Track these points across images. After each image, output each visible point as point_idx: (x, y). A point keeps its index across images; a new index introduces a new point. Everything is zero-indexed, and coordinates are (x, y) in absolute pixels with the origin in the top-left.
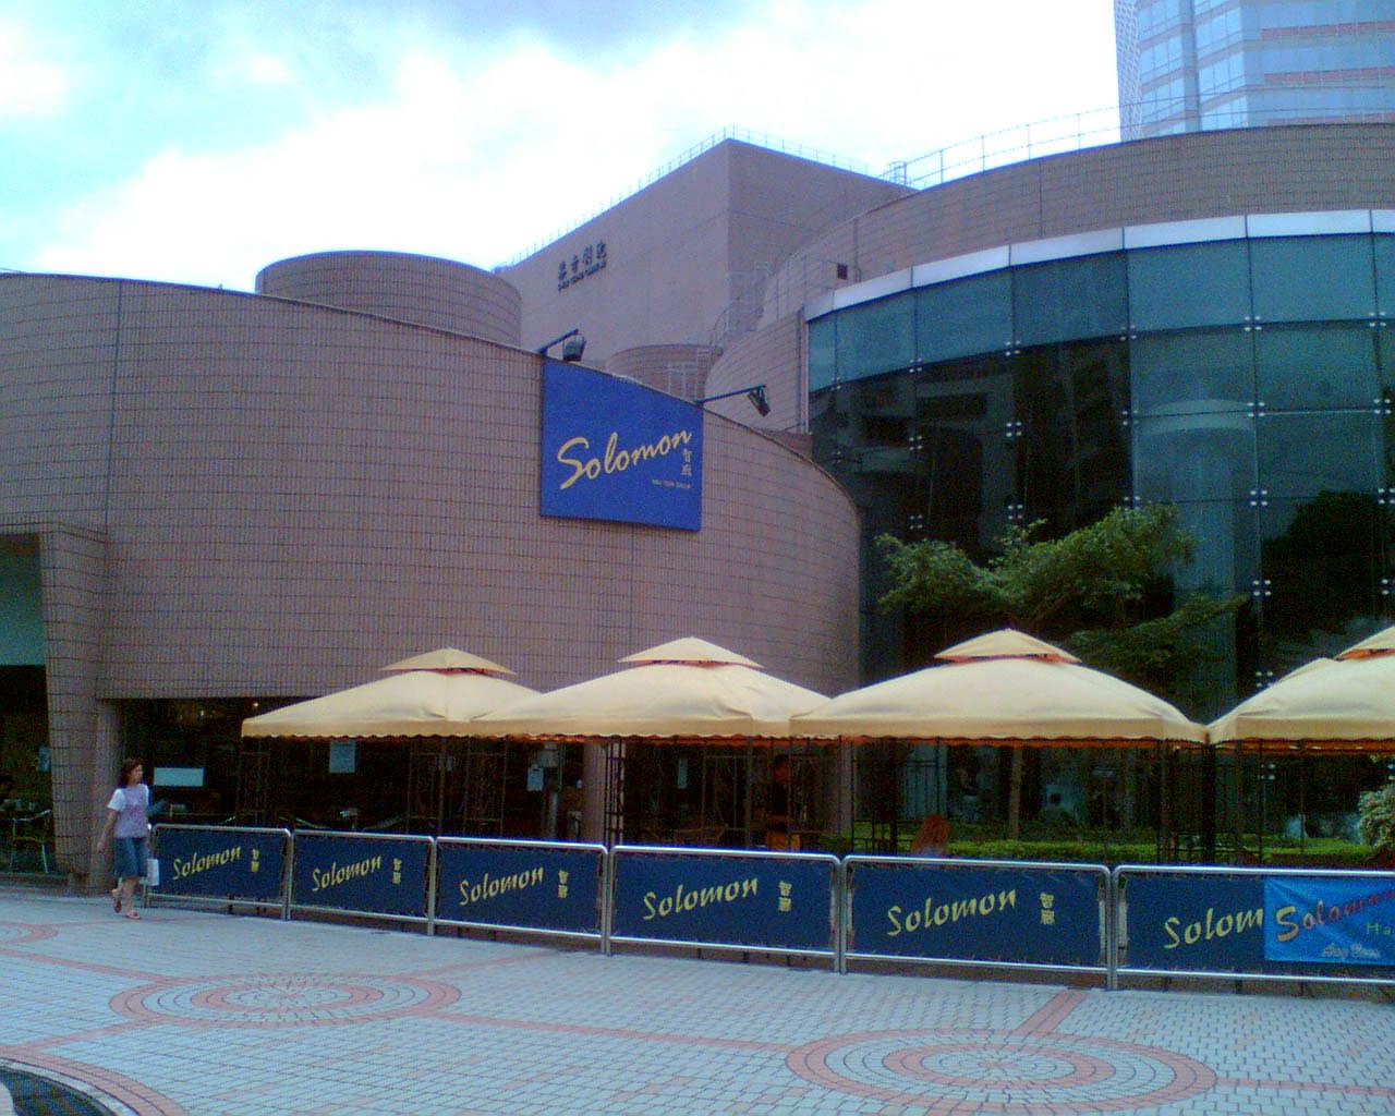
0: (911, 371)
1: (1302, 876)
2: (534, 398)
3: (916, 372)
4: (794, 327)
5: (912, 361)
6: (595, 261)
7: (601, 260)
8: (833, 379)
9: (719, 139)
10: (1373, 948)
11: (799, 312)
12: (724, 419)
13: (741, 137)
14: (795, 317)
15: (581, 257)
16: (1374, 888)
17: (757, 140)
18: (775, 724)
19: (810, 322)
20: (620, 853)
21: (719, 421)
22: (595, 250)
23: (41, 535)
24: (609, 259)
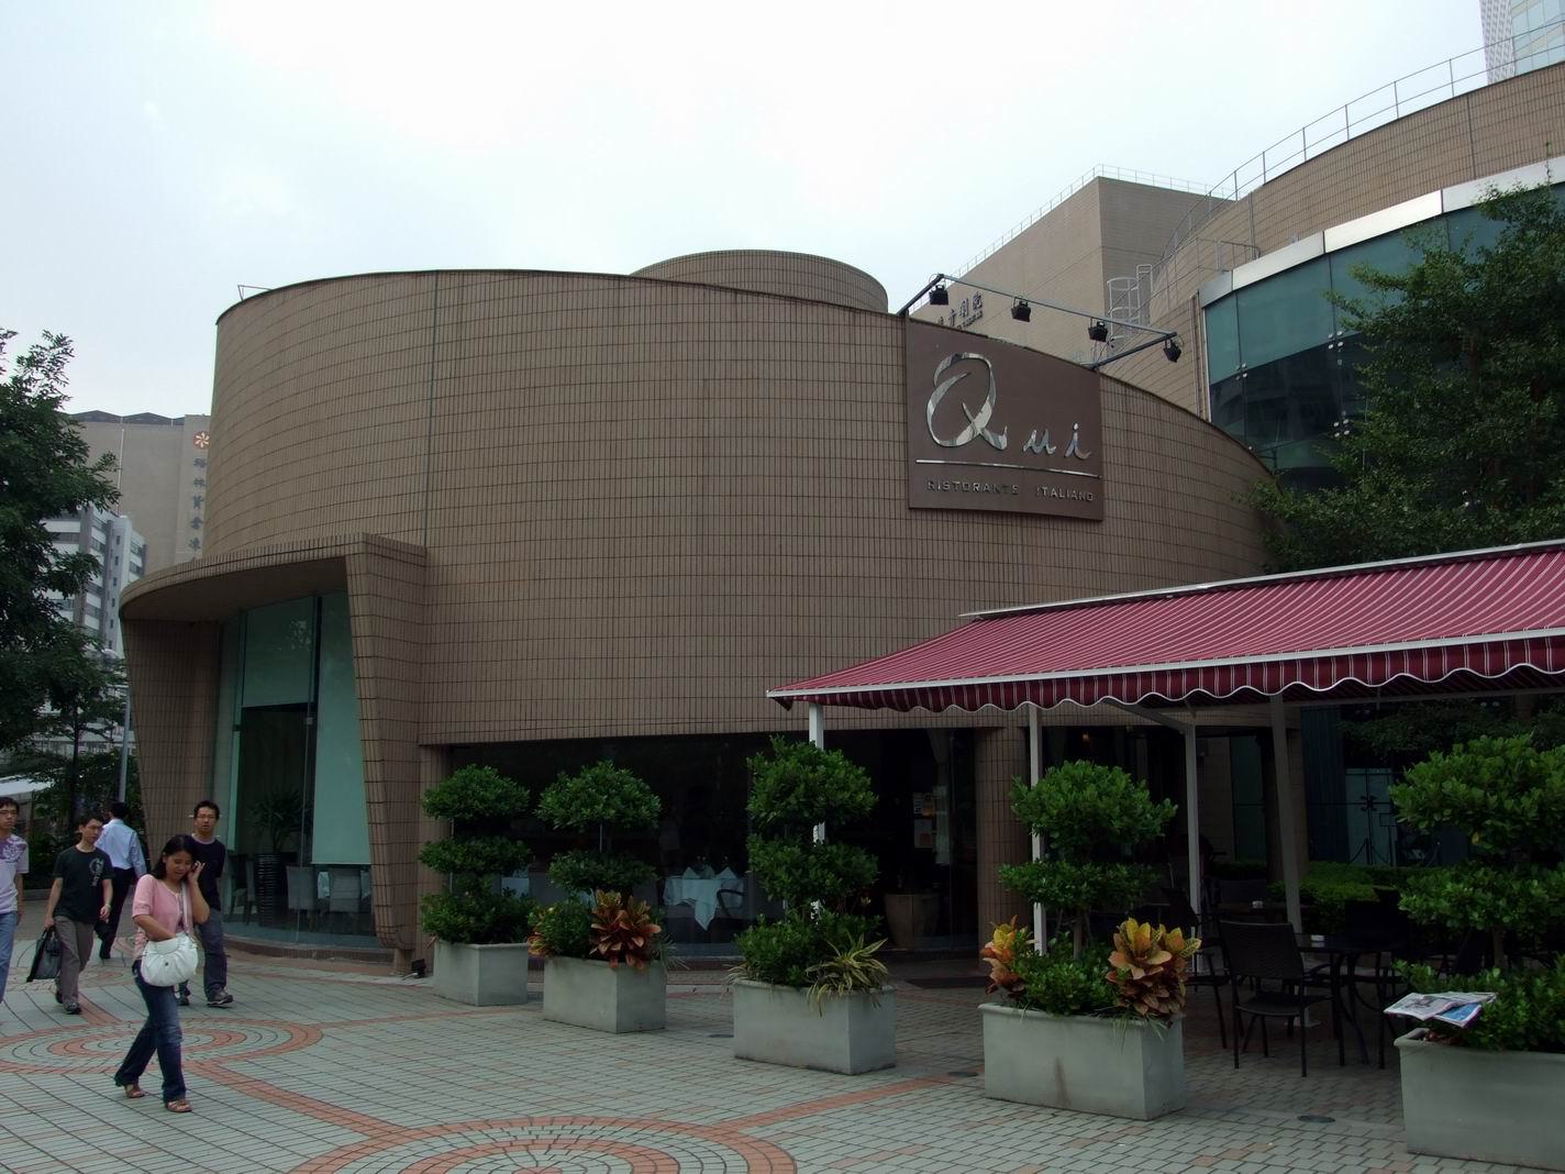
0: (1331, 346)
2: (895, 368)
3: (1336, 347)
4: (1189, 315)
5: (1331, 336)
6: (972, 313)
7: (978, 311)
8: (1238, 367)
9: (1089, 179)
10: (140, 533)
11: (1194, 298)
12: (1126, 385)
13: (1111, 174)
14: (1190, 305)
15: (958, 312)
16: (45, 595)
17: (1127, 176)
18: (133, 892)
19: (1207, 308)
21: (1120, 389)
22: (971, 301)
23: (347, 558)
24: (984, 309)
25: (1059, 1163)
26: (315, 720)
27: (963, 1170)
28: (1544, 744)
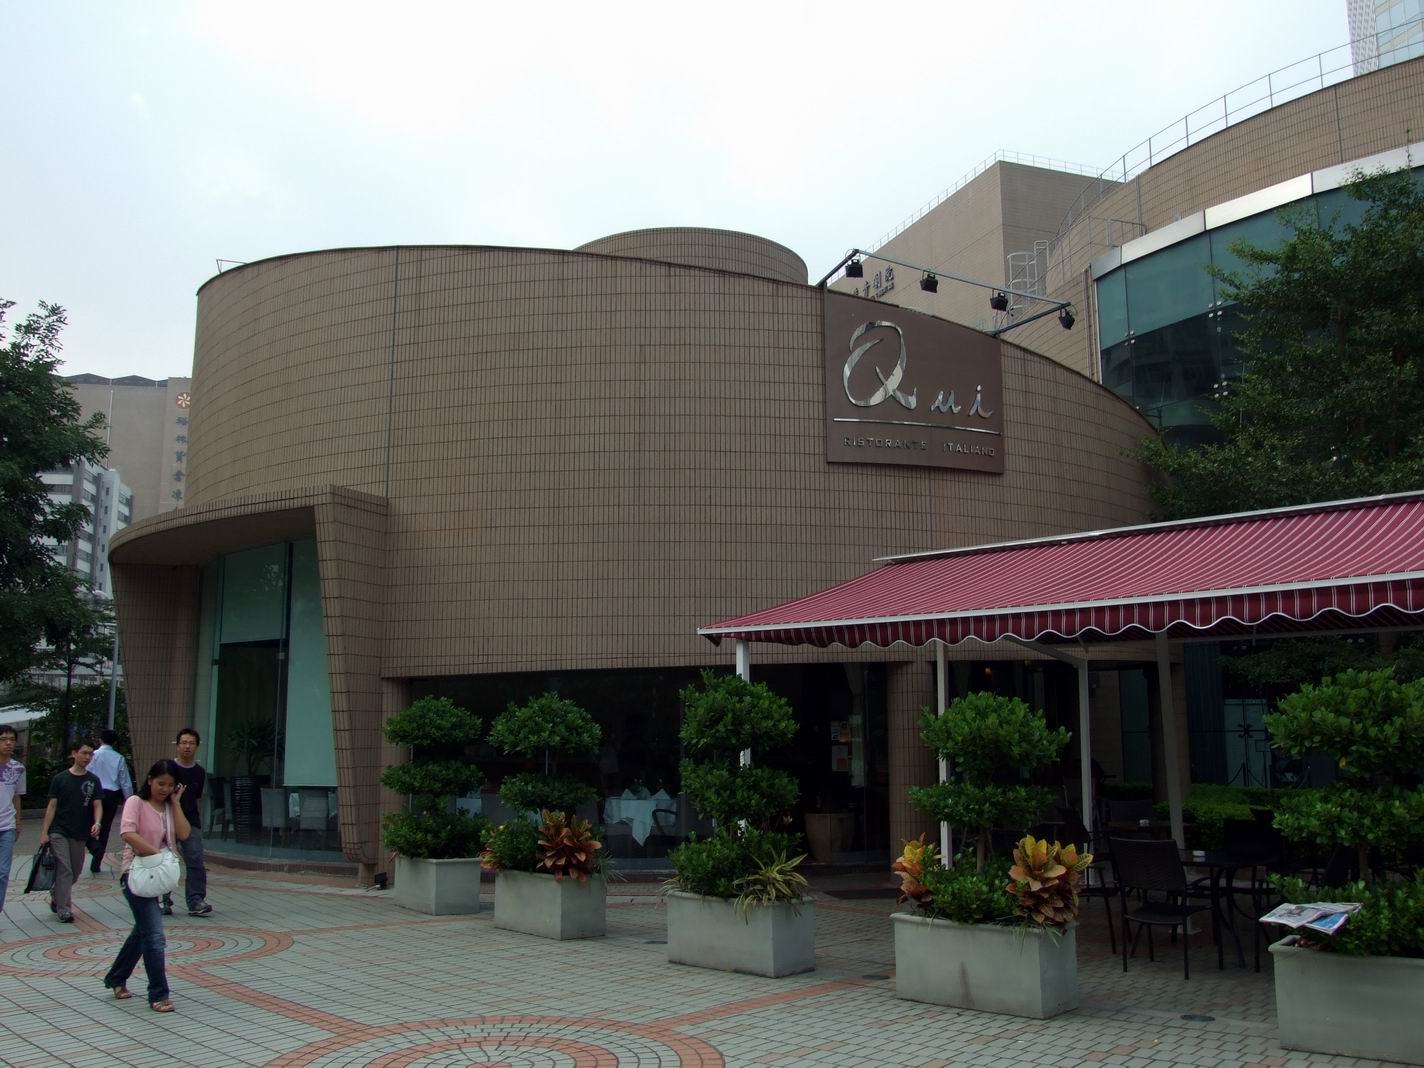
0: (1211, 315)
1: (458, 863)
2: (814, 335)
3: (1215, 316)
4: (1082, 286)
5: (1211, 306)
6: (885, 284)
7: (890, 283)
8: (1126, 334)
9: (991, 163)
10: (128, 485)
11: (1086, 271)
12: (1025, 350)
13: (1011, 158)
14: (1083, 277)
15: (872, 284)
17: (1026, 160)
18: (121, 812)
19: (1098, 280)
20: (91, 809)
21: (1019, 353)
22: (884, 274)
23: (316, 508)
24: (895, 281)
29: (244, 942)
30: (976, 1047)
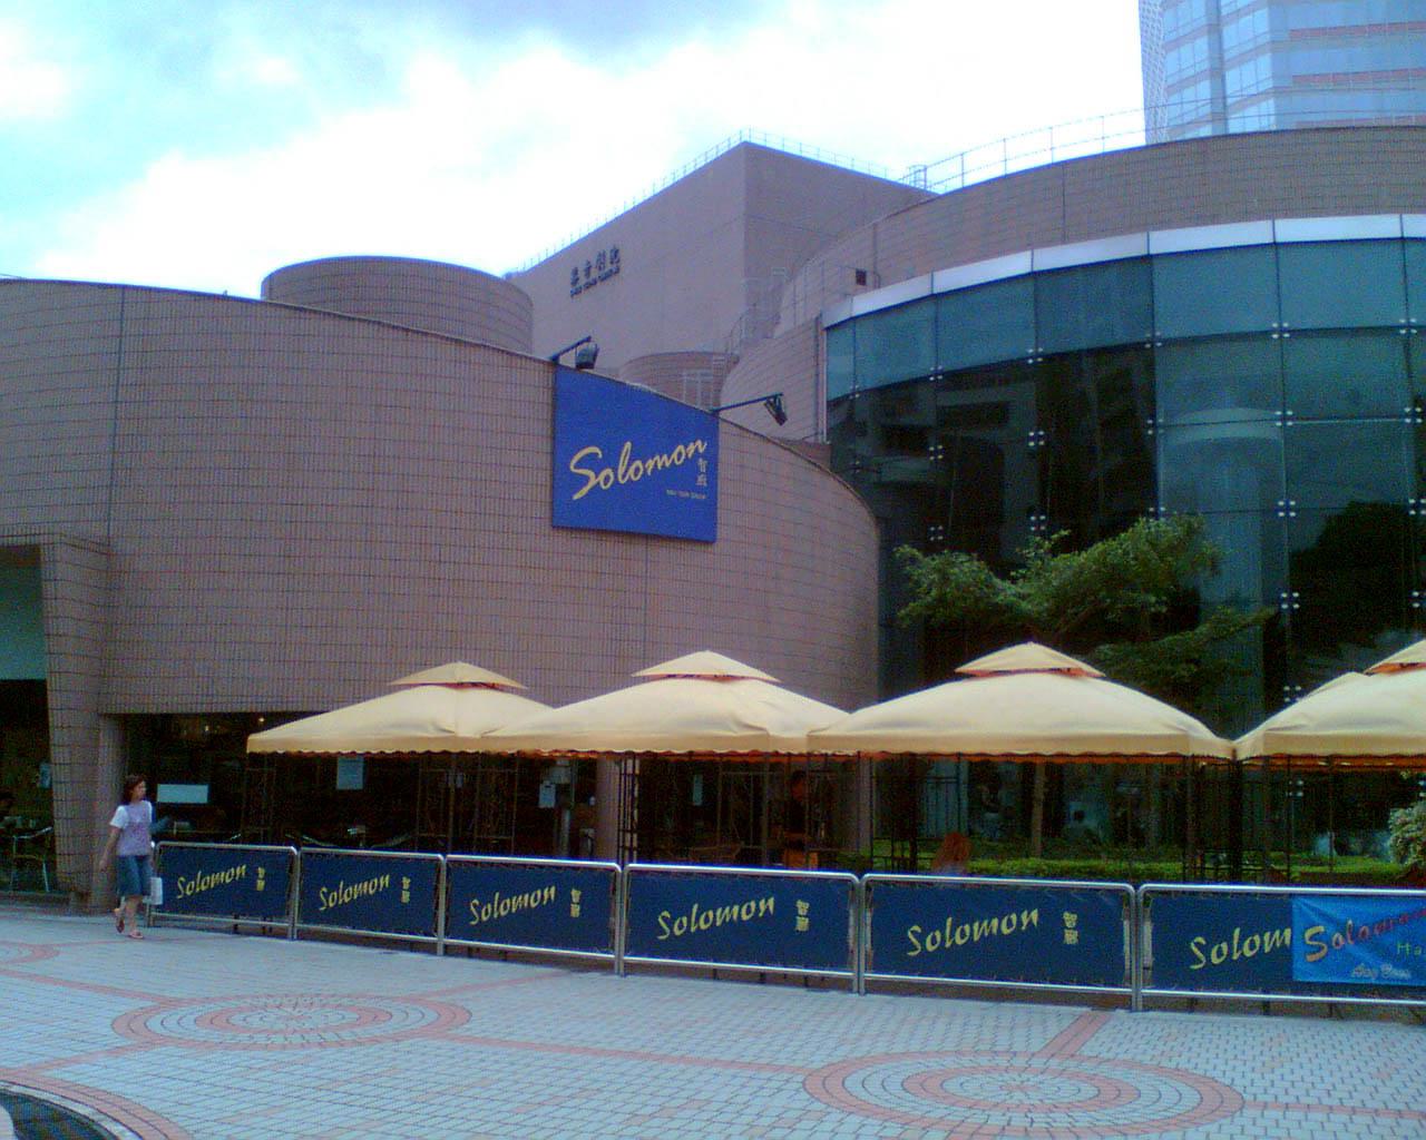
0: (932, 379)
2: (545, 406)
3: (936, 380)
4: (811, 334)
5: (932, 369)
6: (609, 267)
7: (615, 265)
8: (851, 387)
9: (735, 142)
10: (1404, 968)
11: (817, 319)
12: (741, 428)
13: (758, 140)
14: (812, 324)
15: (594, 263)
17: (774, 143)
19: (828, 329)
21: (735, 430)
22: (608, 256)
23: (42, 547)
24: (622, 265)
25: (610, 1129)
26: (1203, 757)
27: (547, 1133)
28: (1424, 904)
29: (414, 1016)
30: (703, 1096)
